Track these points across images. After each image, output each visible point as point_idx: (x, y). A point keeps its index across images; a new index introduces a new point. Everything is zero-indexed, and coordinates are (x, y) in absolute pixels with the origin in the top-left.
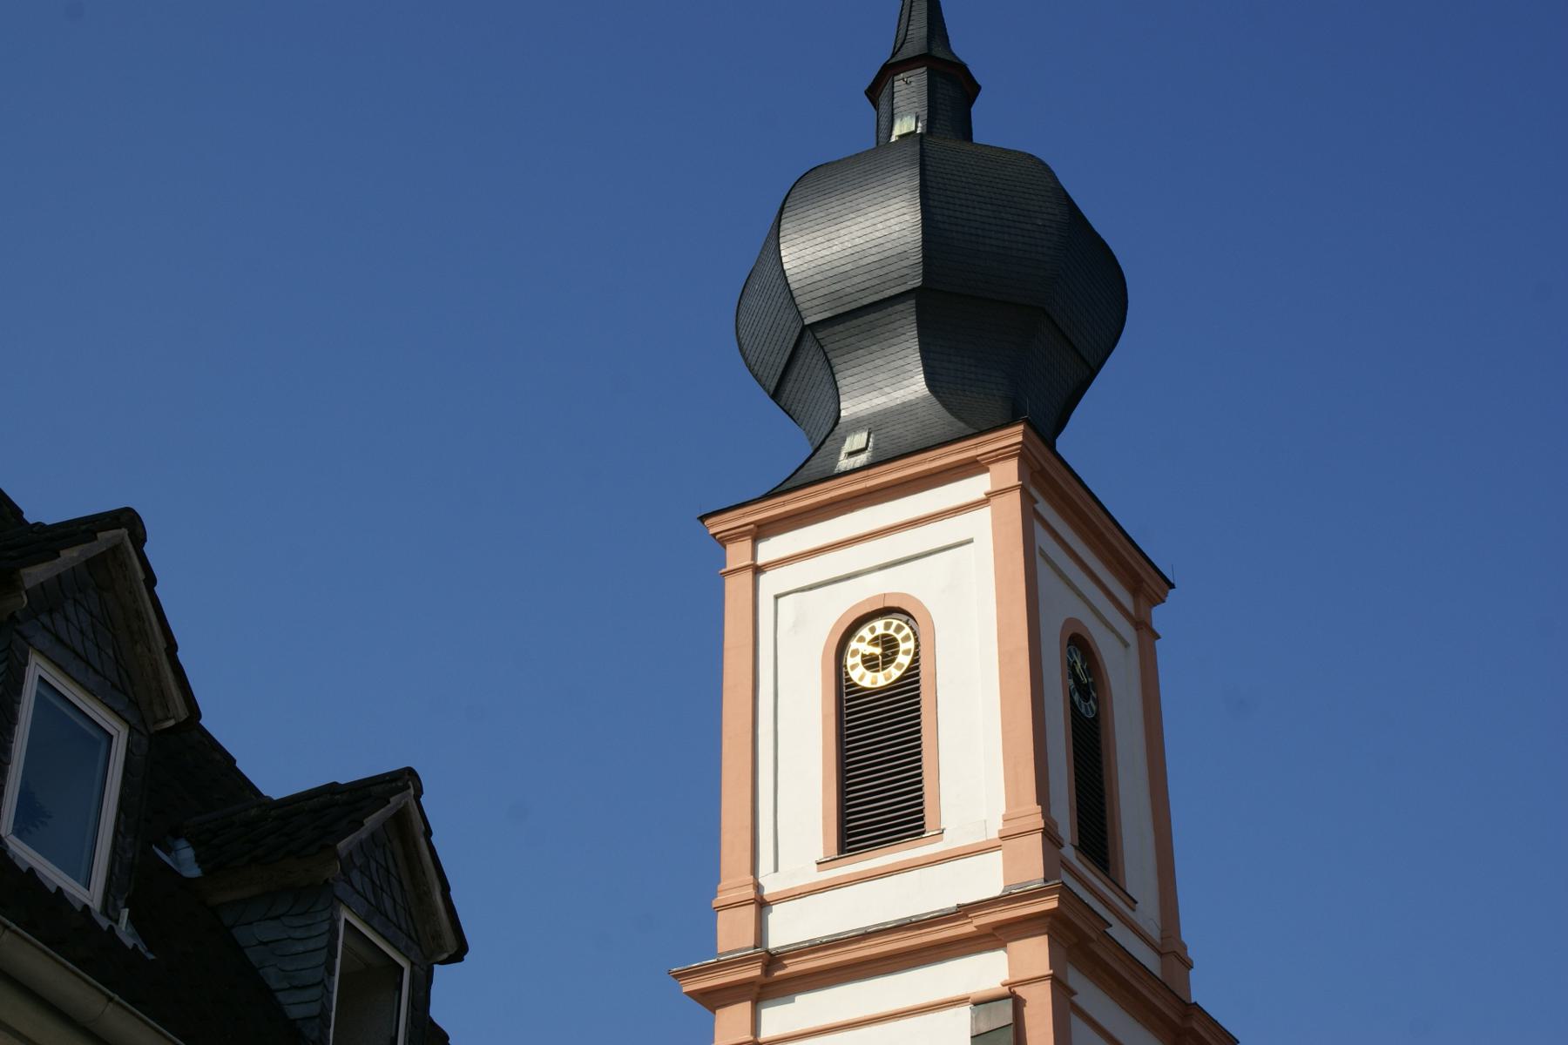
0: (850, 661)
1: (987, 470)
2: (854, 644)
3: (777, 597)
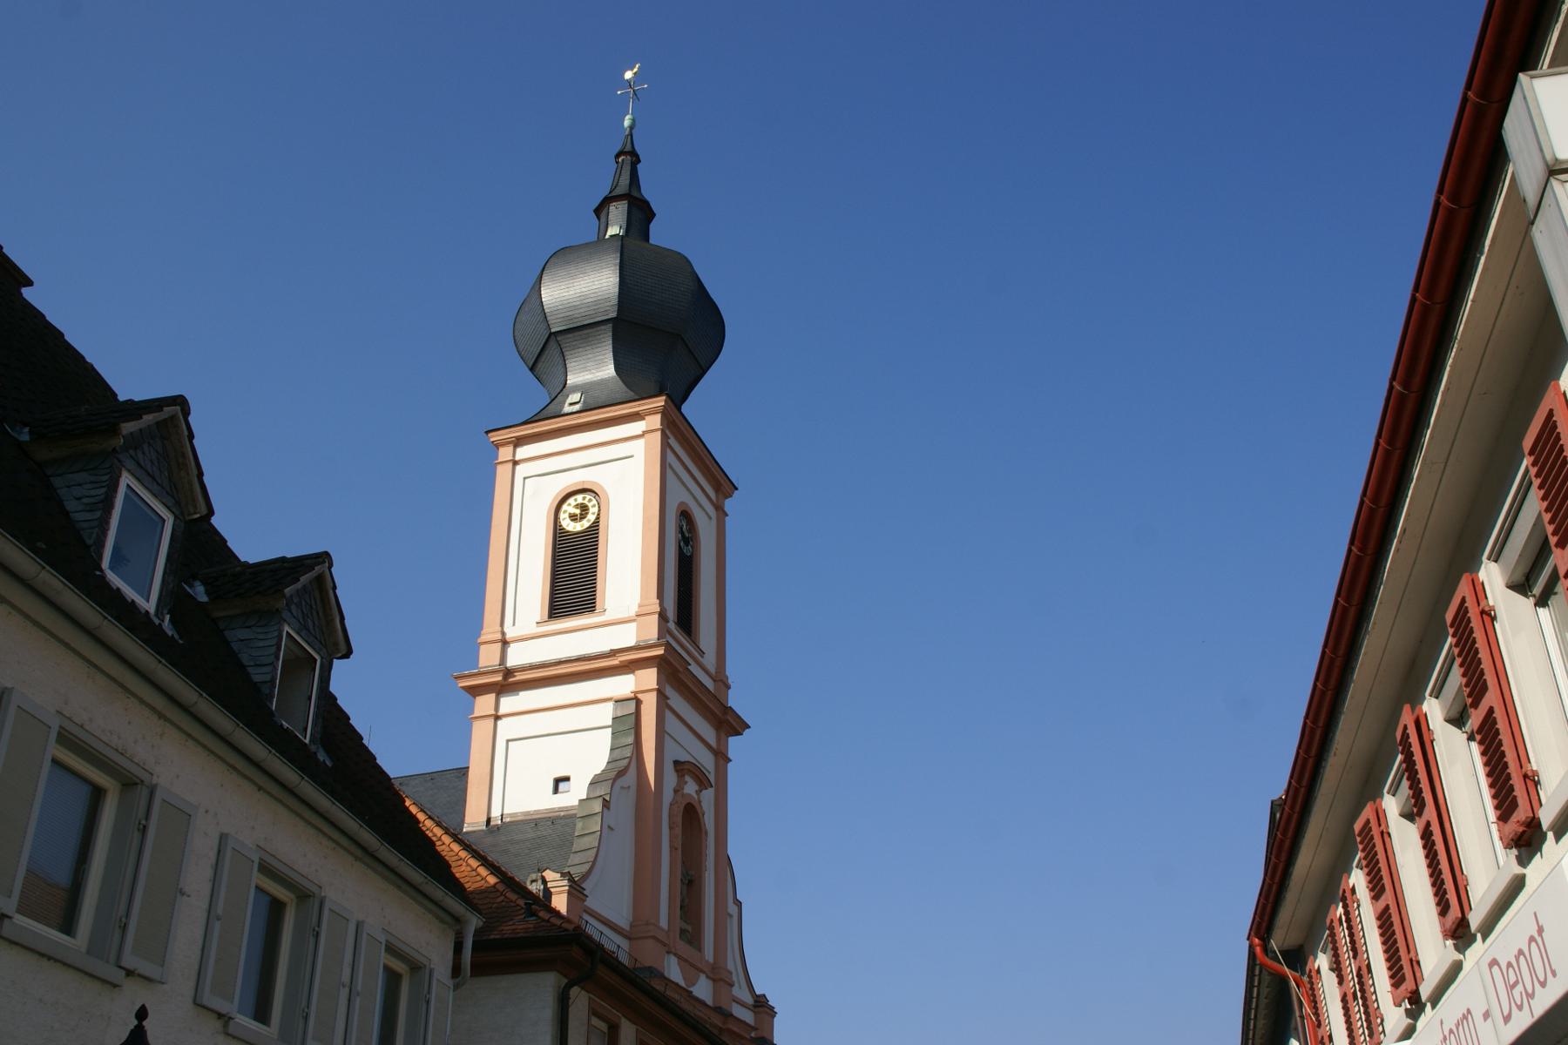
1: (644, 419)
2: (565, 507)
3: (525, 478)
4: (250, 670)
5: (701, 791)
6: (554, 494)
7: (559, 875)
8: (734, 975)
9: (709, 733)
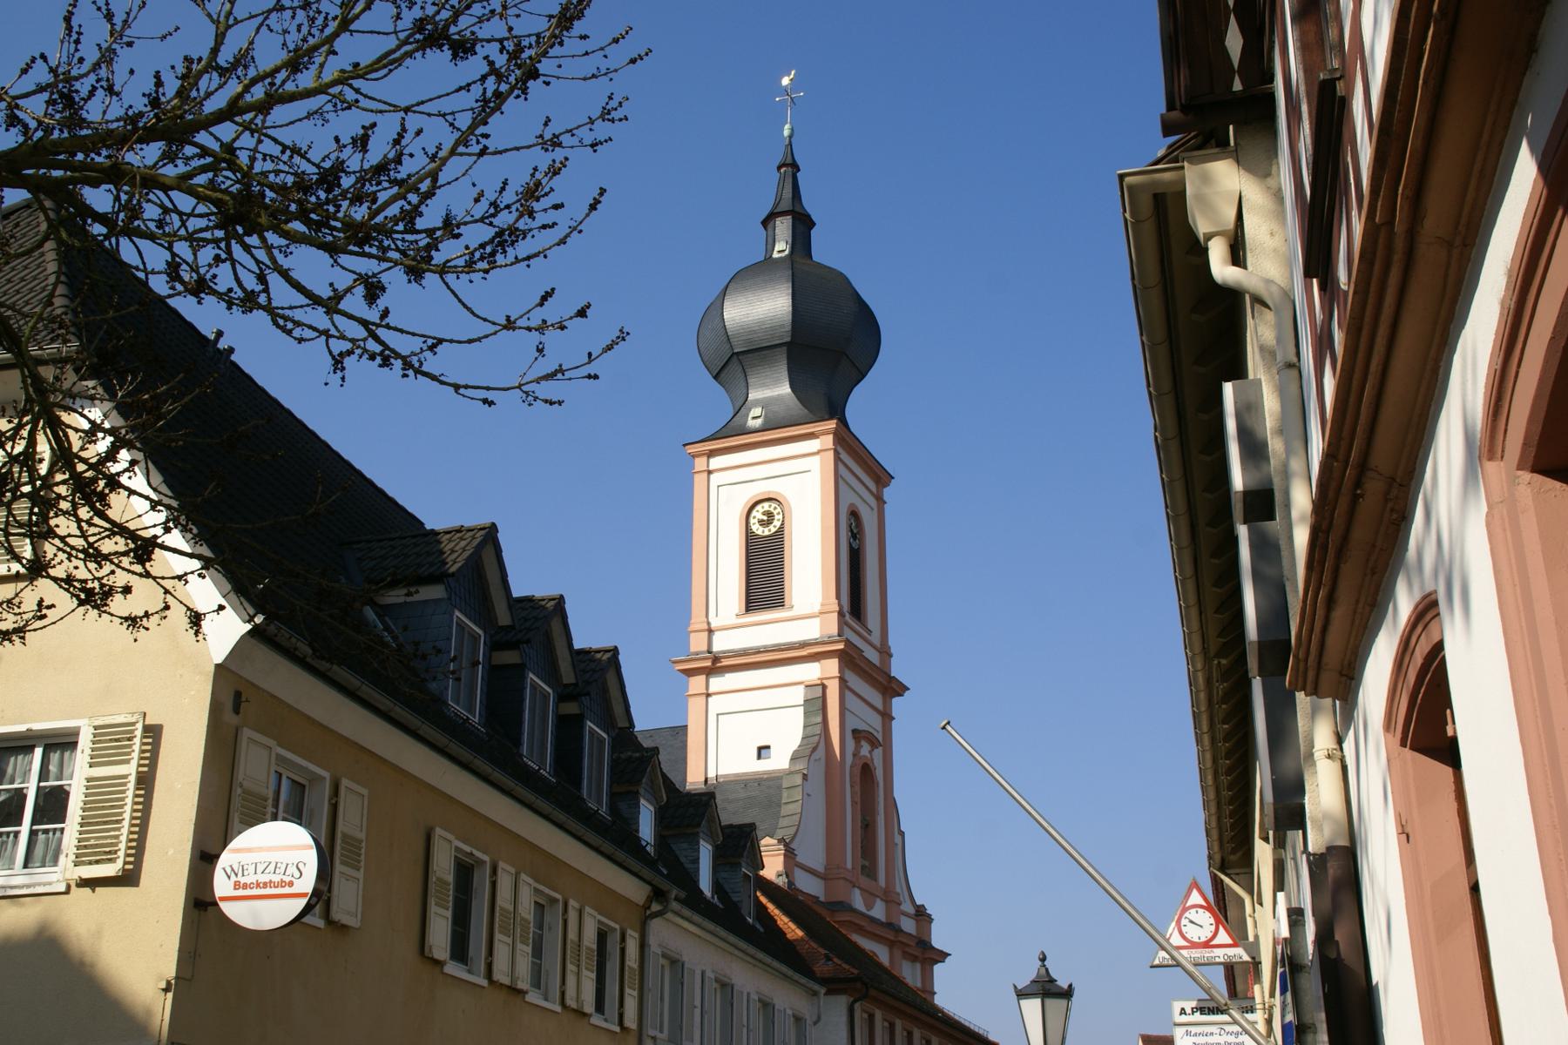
0: (752, 521)
1: (818, 438)
2: (754, 513)
3: (718, 486)
4: (731, 895)
5: (873, 750)
6: (745, 500)
7: (776, 841)
8: (901, 896)
9: (876, 698)
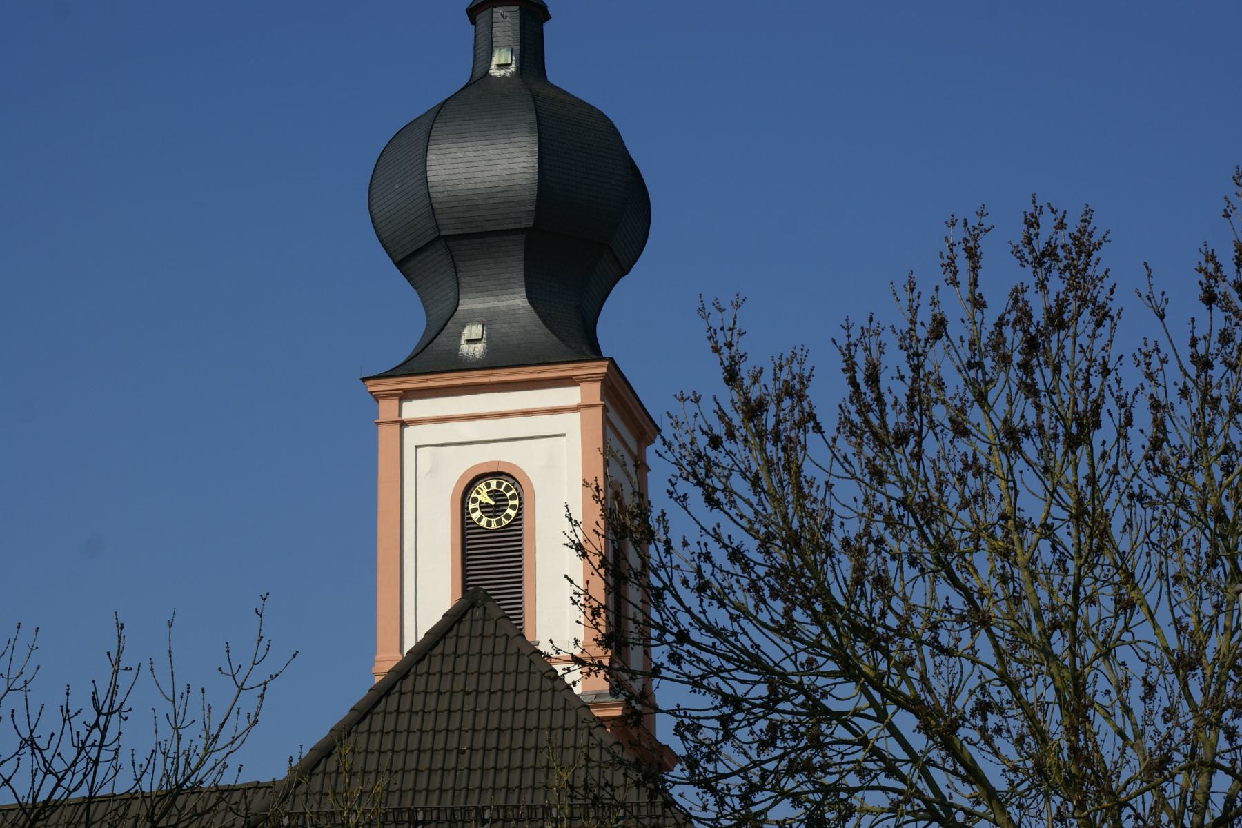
1: (578, 385)
3: (417, 447)
